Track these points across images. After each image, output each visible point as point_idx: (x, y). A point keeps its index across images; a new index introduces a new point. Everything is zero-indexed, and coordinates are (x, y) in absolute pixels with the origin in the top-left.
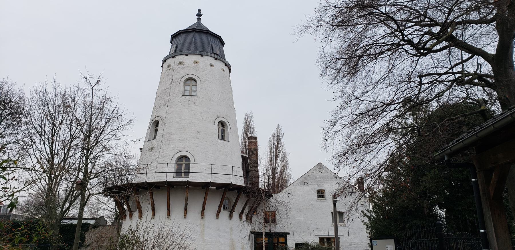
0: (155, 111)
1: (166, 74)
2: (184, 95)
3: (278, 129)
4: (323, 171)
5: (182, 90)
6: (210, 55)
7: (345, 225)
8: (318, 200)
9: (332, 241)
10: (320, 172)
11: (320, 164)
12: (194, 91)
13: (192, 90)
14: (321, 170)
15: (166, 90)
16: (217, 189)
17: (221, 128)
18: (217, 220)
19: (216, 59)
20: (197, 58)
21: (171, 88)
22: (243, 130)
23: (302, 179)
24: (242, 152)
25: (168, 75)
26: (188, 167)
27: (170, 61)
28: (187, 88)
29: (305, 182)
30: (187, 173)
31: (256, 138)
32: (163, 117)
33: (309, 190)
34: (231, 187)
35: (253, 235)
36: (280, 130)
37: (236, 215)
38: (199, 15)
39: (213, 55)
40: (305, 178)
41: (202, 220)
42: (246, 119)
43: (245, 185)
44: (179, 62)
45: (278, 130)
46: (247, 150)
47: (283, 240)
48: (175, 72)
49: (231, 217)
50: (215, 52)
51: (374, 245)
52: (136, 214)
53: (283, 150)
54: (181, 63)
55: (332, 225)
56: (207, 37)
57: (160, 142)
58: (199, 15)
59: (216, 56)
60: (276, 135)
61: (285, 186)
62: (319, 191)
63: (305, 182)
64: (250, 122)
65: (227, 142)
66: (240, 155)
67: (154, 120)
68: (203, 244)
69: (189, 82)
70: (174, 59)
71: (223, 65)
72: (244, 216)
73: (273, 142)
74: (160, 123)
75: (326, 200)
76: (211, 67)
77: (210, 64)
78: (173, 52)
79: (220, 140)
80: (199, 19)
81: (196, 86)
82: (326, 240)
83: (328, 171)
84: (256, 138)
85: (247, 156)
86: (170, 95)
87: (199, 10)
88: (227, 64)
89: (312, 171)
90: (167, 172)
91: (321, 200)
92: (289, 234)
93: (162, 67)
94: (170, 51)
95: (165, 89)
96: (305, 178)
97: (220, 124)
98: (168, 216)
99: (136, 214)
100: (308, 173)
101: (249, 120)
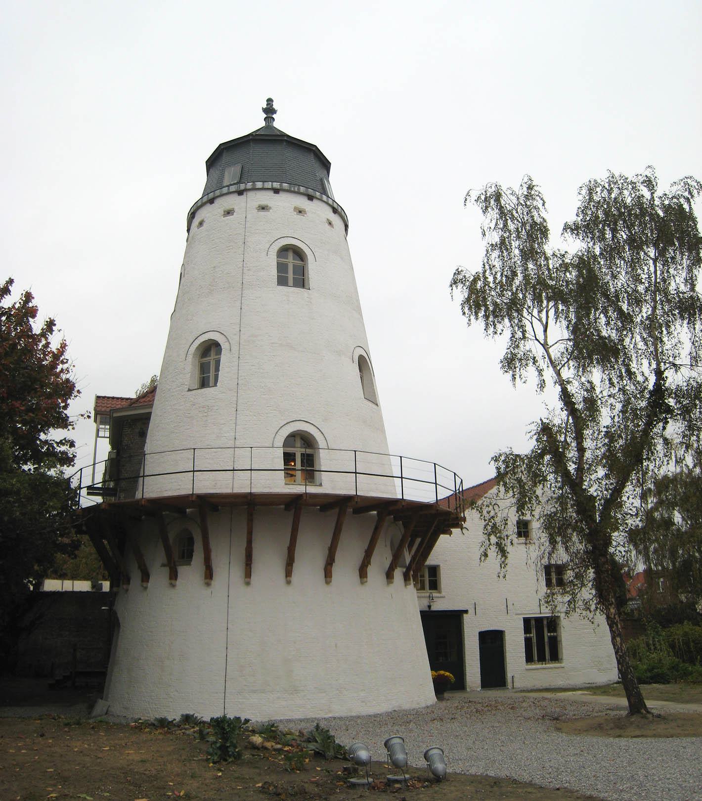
37: (375, 572)
38: (269, 111)
44: (259, 207)
51: (477, 646)
56: (290, 153)
58: (269, 111)
62: (301, 281)
88: (336, 210)
90: (194, 471)
92: (466, 612)
93: (188, 231)
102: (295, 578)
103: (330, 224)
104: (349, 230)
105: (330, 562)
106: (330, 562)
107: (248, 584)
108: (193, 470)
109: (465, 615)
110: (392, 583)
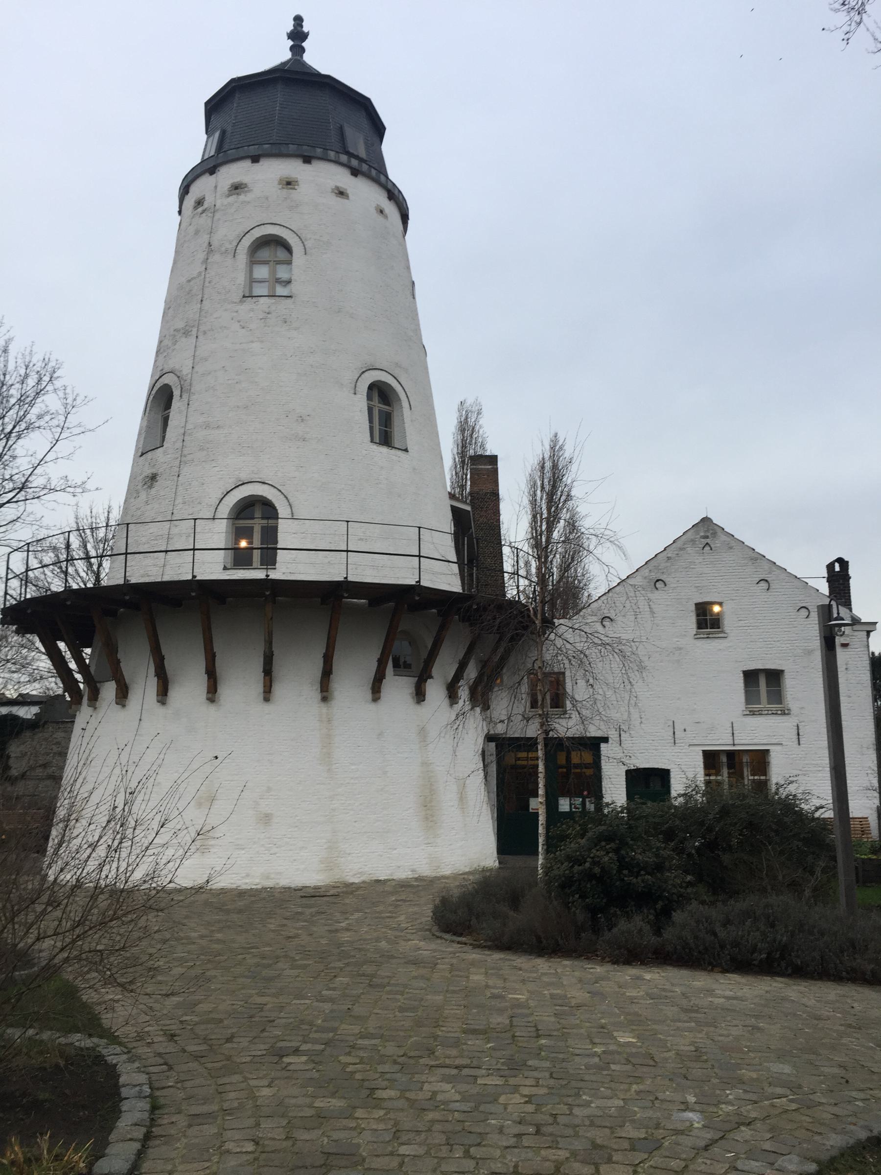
0: (161, 357)
1: (192, 230)
2: (249, 296)
3: (555, 446)
4: (716, 543)
5: (241, 278)
6: (333, 158)
7: (786, 712)
8: (698, 636)
9: (744, 760)
10: (707, 548)
11: (706, 521)
12: (284, 282)
13: (278, 281)
14: (708, 541)
15: (192, 283)
16: (370, 604)
17: (378, 406)
18: (373, 707)
19: (355, 173)
20: (292, 168)
21: (207, 276)
22: (455, 451)
23: (647, 571)
24: (452, 496)
25: (197, 232)
26: (270, 534)
27: (203, 186)
28: (261, 272)
29: (658, 581)
30: (269, 558)
31: (493, 459)
32: (186, 371)
33: (669, 603)
34: (417, 598)
35: (493, 745)
36: (561, 448)
37: (435, 690)
38: (298, 36)
39: (344, 158)
40: (657, 568)
41: (322, 704)
42: (462, 419)
43: (464, 591)
44: (232, 186)
45: (554, 451)
46: (467, 470)
47: (588, 758)
48: (219, 219)
49: (420, 695)
50: (351, 151)
52: (109, 690)
53: (570, 504)
54: (237, 188)
55: (745, 713)
57: (178, 455)
58: (298, 36)
59: (354, 163)
60: (548, 465)
61: (576, 605)
63: (658, 581)
64: (473, 428)
65: (399, 453)
66: (447, 503)
67: (158, 386)
68: (329, 784)
69: (265, 253)
70: (214, 175)
71: (379, 197)
72: (464, 693)
73: (539, 483)
74: (176, 393)
75: (725, 635)
76: (340, 200)
77: (337, 188)
78: (212, 153)
79: (374, 447)
80: (298, 50)
81: (289, 267)
82: (724, 759)
83: (733, 544)
84: (493, 459)
85: (468, 508)
86: (204, 299)
87: (298, 20)
88: (394, 195)
89: (679, 544)
91: (710, 636)
92: (605, 740)
93: (180, 212)
94: (204, 152)
95: (189, 281)
96: (657, 568)
97: (377, 395)
98: (210, 695)
99: (109, 690)
100: (665, 552)
101: (471, 421)
102: (279, 690)
103: (381, 212)
104: (410, 223)
105: (327, 674)
106: (327, 674)
107: (267, 699)
108: (128, 556)
109: (603, 746)
110: (424, 700)
